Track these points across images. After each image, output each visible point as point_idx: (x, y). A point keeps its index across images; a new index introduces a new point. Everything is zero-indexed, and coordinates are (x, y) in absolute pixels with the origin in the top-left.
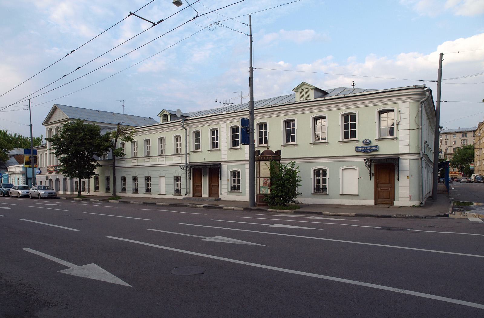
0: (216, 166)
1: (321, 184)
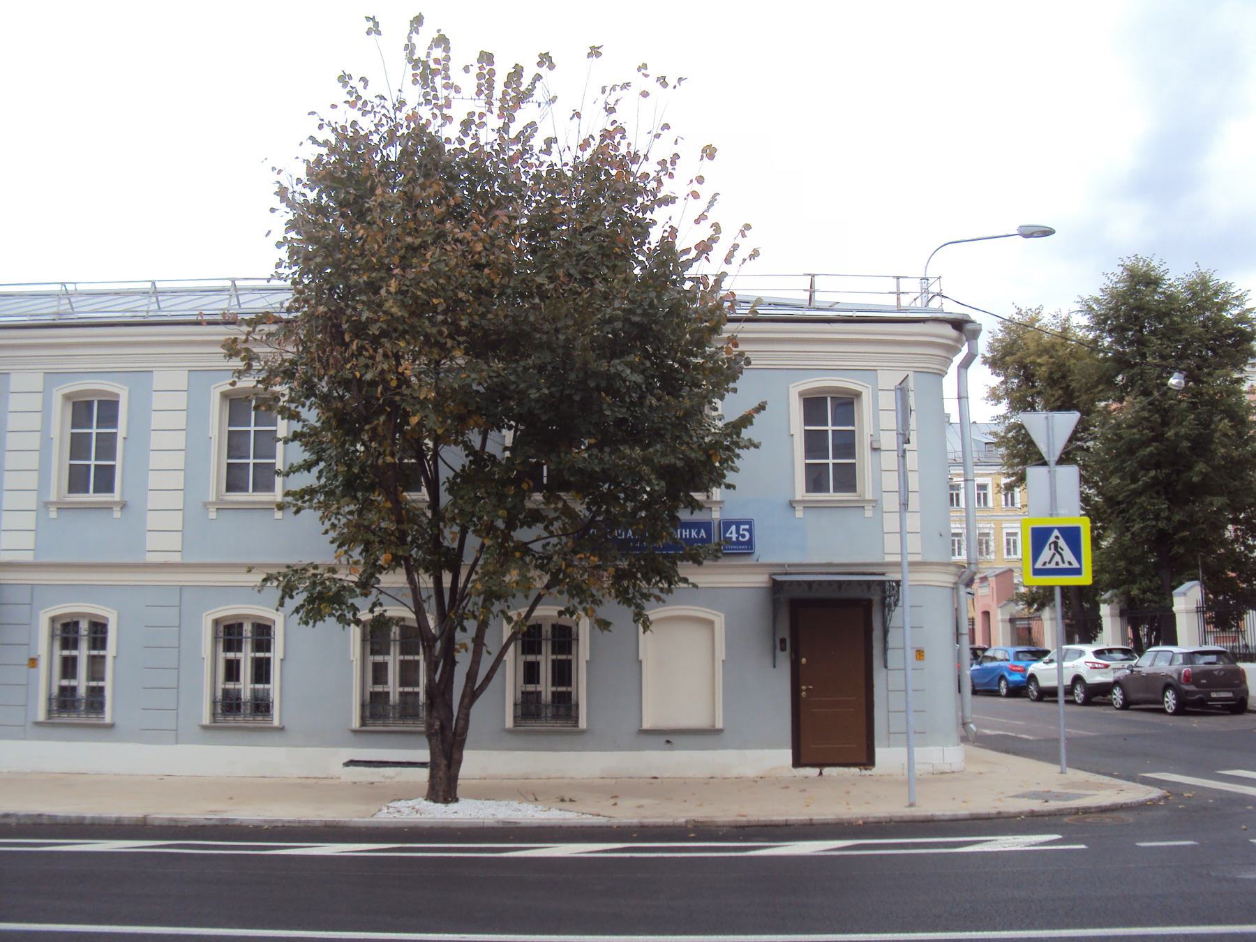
1: (82, 683)
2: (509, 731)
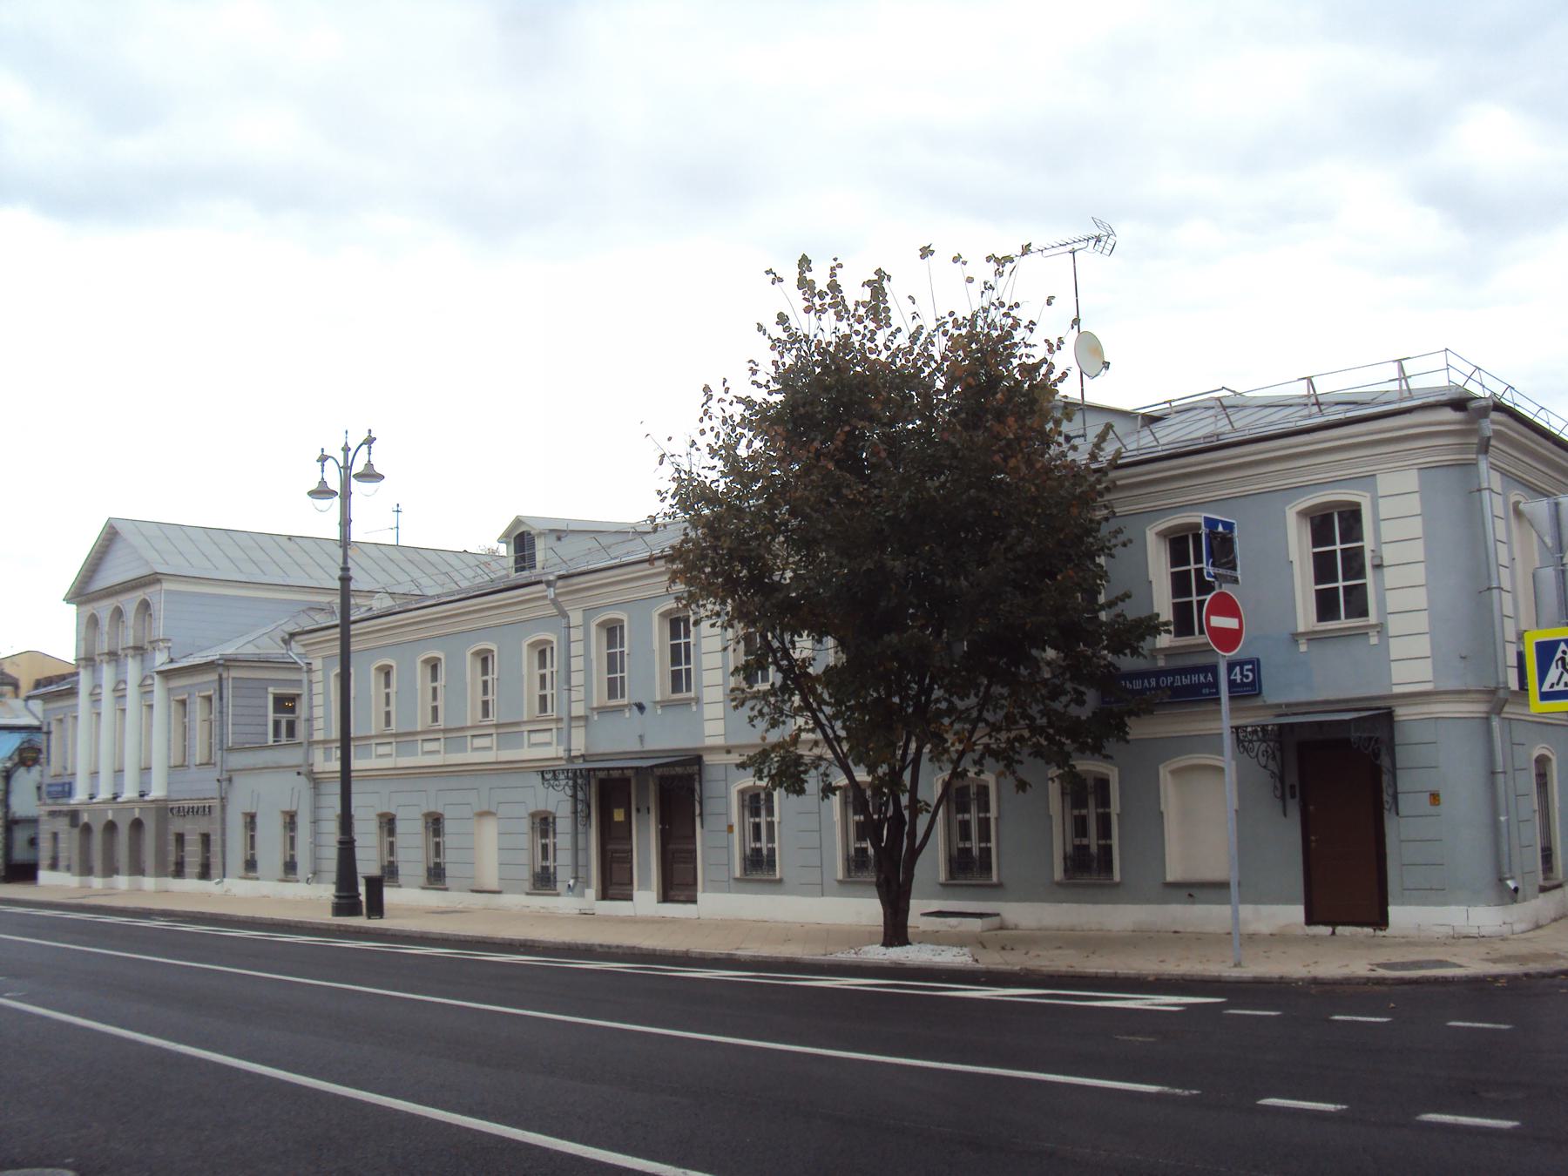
0: (679, 770)
1: (1093, 841)
2: (1059, 884)
